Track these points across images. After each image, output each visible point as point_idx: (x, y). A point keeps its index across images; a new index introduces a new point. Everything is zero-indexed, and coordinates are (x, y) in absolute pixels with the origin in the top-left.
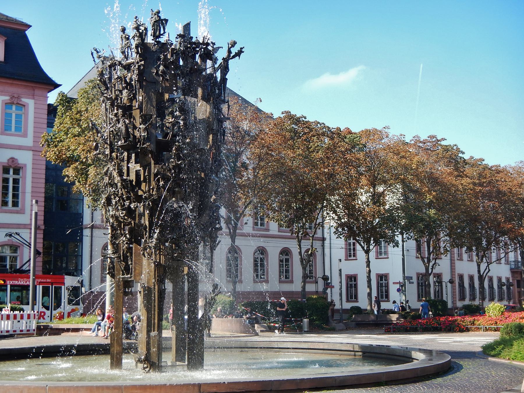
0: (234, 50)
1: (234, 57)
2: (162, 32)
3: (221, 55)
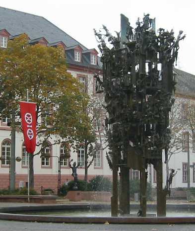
0: (182, 36)
1: (181, 39)
2: (149, 26)
3: (176, 36)
